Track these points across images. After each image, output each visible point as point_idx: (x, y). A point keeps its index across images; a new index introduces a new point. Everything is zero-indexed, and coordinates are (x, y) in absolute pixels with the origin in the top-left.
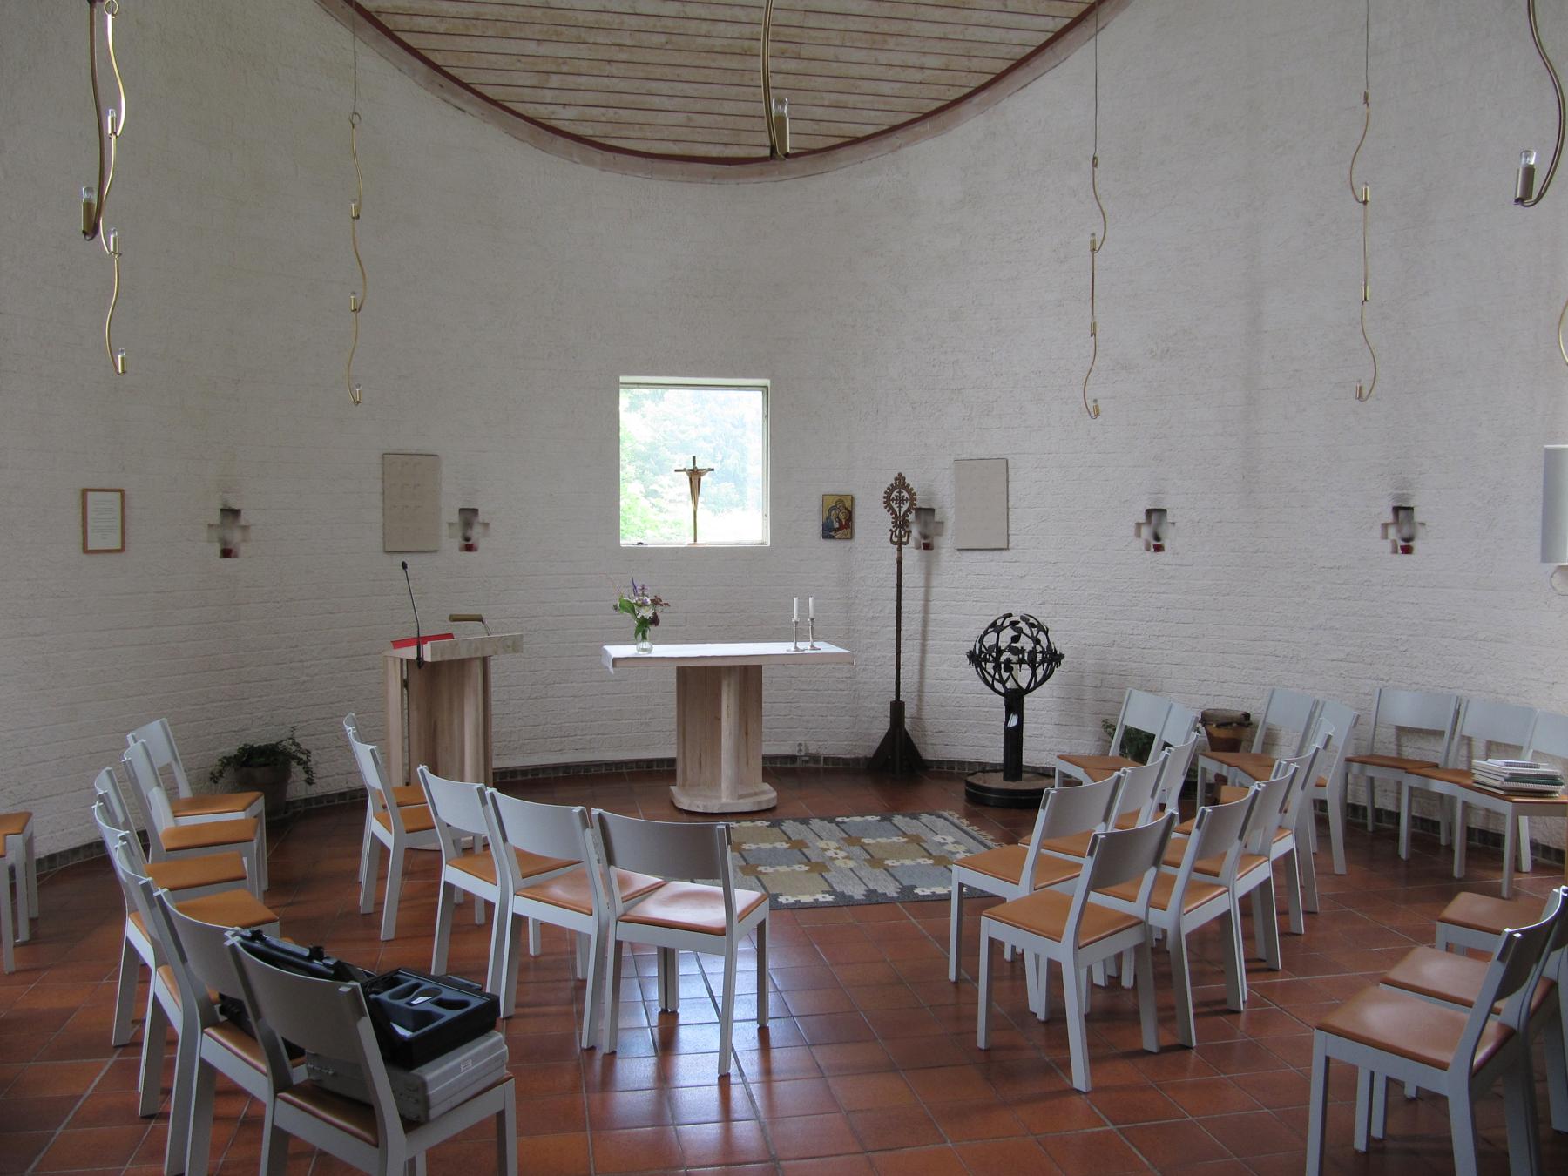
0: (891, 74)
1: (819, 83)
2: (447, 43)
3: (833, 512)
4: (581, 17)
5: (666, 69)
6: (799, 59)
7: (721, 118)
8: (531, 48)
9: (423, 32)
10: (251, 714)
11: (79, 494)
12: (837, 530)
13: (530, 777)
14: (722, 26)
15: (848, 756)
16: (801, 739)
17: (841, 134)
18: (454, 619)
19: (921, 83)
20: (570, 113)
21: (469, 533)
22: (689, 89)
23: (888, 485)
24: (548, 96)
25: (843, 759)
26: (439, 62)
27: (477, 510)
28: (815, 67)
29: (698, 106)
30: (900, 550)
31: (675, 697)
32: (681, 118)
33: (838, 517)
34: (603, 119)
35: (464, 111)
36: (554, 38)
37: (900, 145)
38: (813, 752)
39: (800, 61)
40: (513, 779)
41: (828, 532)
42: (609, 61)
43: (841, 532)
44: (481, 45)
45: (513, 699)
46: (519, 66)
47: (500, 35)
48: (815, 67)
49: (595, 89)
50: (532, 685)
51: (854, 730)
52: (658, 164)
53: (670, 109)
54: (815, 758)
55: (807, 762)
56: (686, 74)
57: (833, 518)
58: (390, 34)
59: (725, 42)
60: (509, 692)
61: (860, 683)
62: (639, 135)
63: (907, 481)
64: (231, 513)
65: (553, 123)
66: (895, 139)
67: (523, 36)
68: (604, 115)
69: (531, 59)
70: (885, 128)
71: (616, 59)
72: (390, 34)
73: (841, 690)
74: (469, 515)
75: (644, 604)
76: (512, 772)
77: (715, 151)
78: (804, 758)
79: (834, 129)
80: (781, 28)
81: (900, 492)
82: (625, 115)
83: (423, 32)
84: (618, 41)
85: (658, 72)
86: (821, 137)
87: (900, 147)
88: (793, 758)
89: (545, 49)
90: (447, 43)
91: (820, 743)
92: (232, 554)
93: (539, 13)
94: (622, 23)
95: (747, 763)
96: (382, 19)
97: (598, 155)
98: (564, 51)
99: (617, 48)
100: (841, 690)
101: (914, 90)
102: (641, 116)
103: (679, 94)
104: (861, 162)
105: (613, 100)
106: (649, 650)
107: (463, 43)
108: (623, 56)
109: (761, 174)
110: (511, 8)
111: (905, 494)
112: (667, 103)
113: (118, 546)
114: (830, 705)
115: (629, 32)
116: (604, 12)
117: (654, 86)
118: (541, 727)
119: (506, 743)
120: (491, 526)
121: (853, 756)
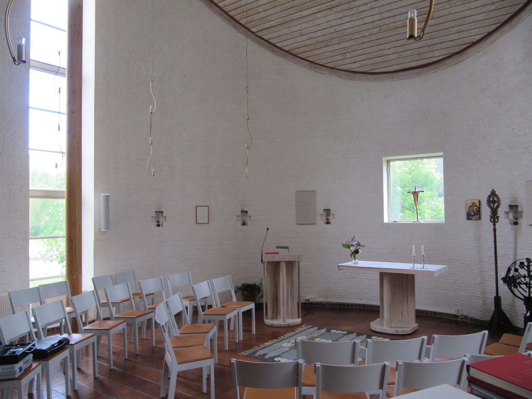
0: (478, 11)
1: (447, 25)
2: (312, 53)
3: (471, 208)
4: (348, 31)
5: (384, 40)
6: (434, 18)
7: (411, 51)
8: (336, 47)
9: (303, 52)
10: (251, 274)
11: (195, 207)
12: (473, 216)
13: (350, 307)
14: (398, 17)
15: (481, 319)
16: (460, 308)
17: (465, 43)
18: (278, 247)
19: (495, 10)
20: (357, 65)
21: (329, 218)
22: (395, 44)
23: (488, 195)
24: (348, 61)
25: (480, 320)
26: (312, 60)
27: (330, 210)
28: (442, 20)
29: (401, 49)
30: (494, 225)
31: (379, 281)
32: (396, 55)
33: (473, 210)
34: (369, 64)
35: (323, 74)
36: (342, 41)
37: (495, 40)
38: (466, 315)
39: (435, 19)
40: (344, 307)
41: (469, 217)
42: (363, 43)
43: (475, 217)
44: (321, 51)
45: (343, 278)
46: (335, 54)
47: (325, 46)
48: (442, 20)
49: (362, 54)
50: (351, 273)
51: (484, 307)
52: (394, 75)
53: (391, 53)
54: (466, 317)
55: (463, 318)
56: (391, 39)
57: (471, 210)
58: (295, 55)
59: (401, 22)
60: (342, 275)
61: (485, 286)
62: (384, 66)
63: (496, 193)
64: (244, 212)
65: (353, 70)
66: (492, 38)
67: (332, 44)
68: (369, 62)
69: (338, 51)
70: (486, 34)
71: (365, 42)
72: (295, 55)
73: (477, 288)
74: (327, 212)
75: (352, 245)
76: (343, 304)
77: (414, 64)
78: (461, 317)
79: (461, 42)
80: (422, 9)
81: (493, 198)
82: (376, 60)
83: (303, 52)
84: (363, 35)
85: (382, 41)
86: (457, 47)
87: (495, 41)
88: (456, 316)
89: (341, 46)
90: (312, 53)
91: (469, 311)
92: (245, 224)
93: (334, 34)
94: (362, 28)
95: (408, 314)
96: (292, 52)
97: (372, 77)
98: (346, 44)
99: (364, 38)
100: (477, 288)
101: (493, 14)
102: (381, 59)
103: (392, 47)
104: (478, 52)
105: (370, 56)
106: (356, 264)
107: (316, 52)
108: (367, 40)
109: (436, 68)
110: (325, 36)
111: (495, 199)
112: (389, 52)
113: (207, 222)
114: (472, 295)
115: (366, 31)
116: (355, 27)
117: (382, 47)
118: (354, 289)
119: (341, 293)
120: (335, 215)
121: (483, 320)
